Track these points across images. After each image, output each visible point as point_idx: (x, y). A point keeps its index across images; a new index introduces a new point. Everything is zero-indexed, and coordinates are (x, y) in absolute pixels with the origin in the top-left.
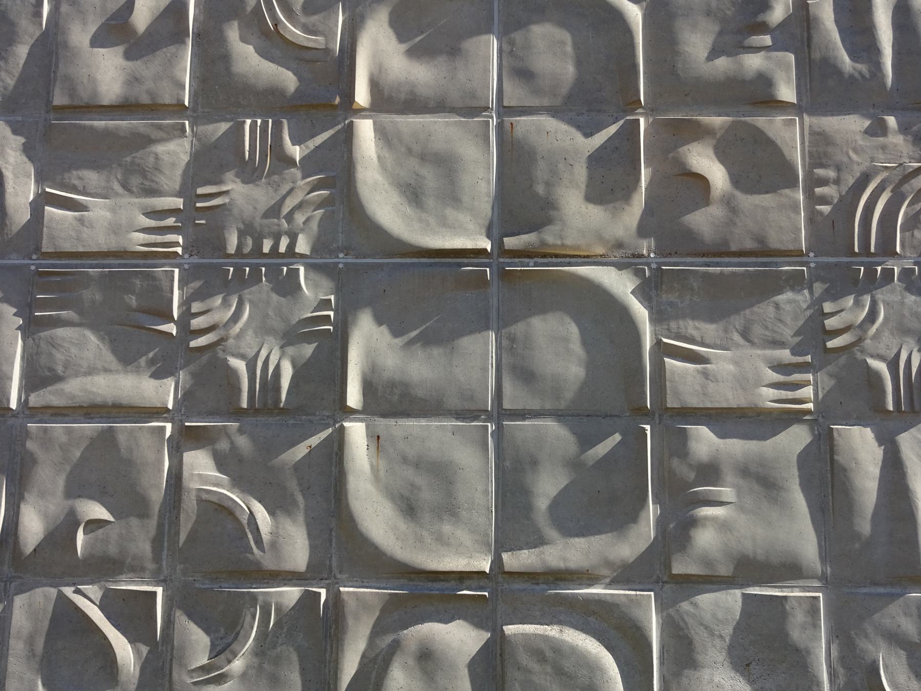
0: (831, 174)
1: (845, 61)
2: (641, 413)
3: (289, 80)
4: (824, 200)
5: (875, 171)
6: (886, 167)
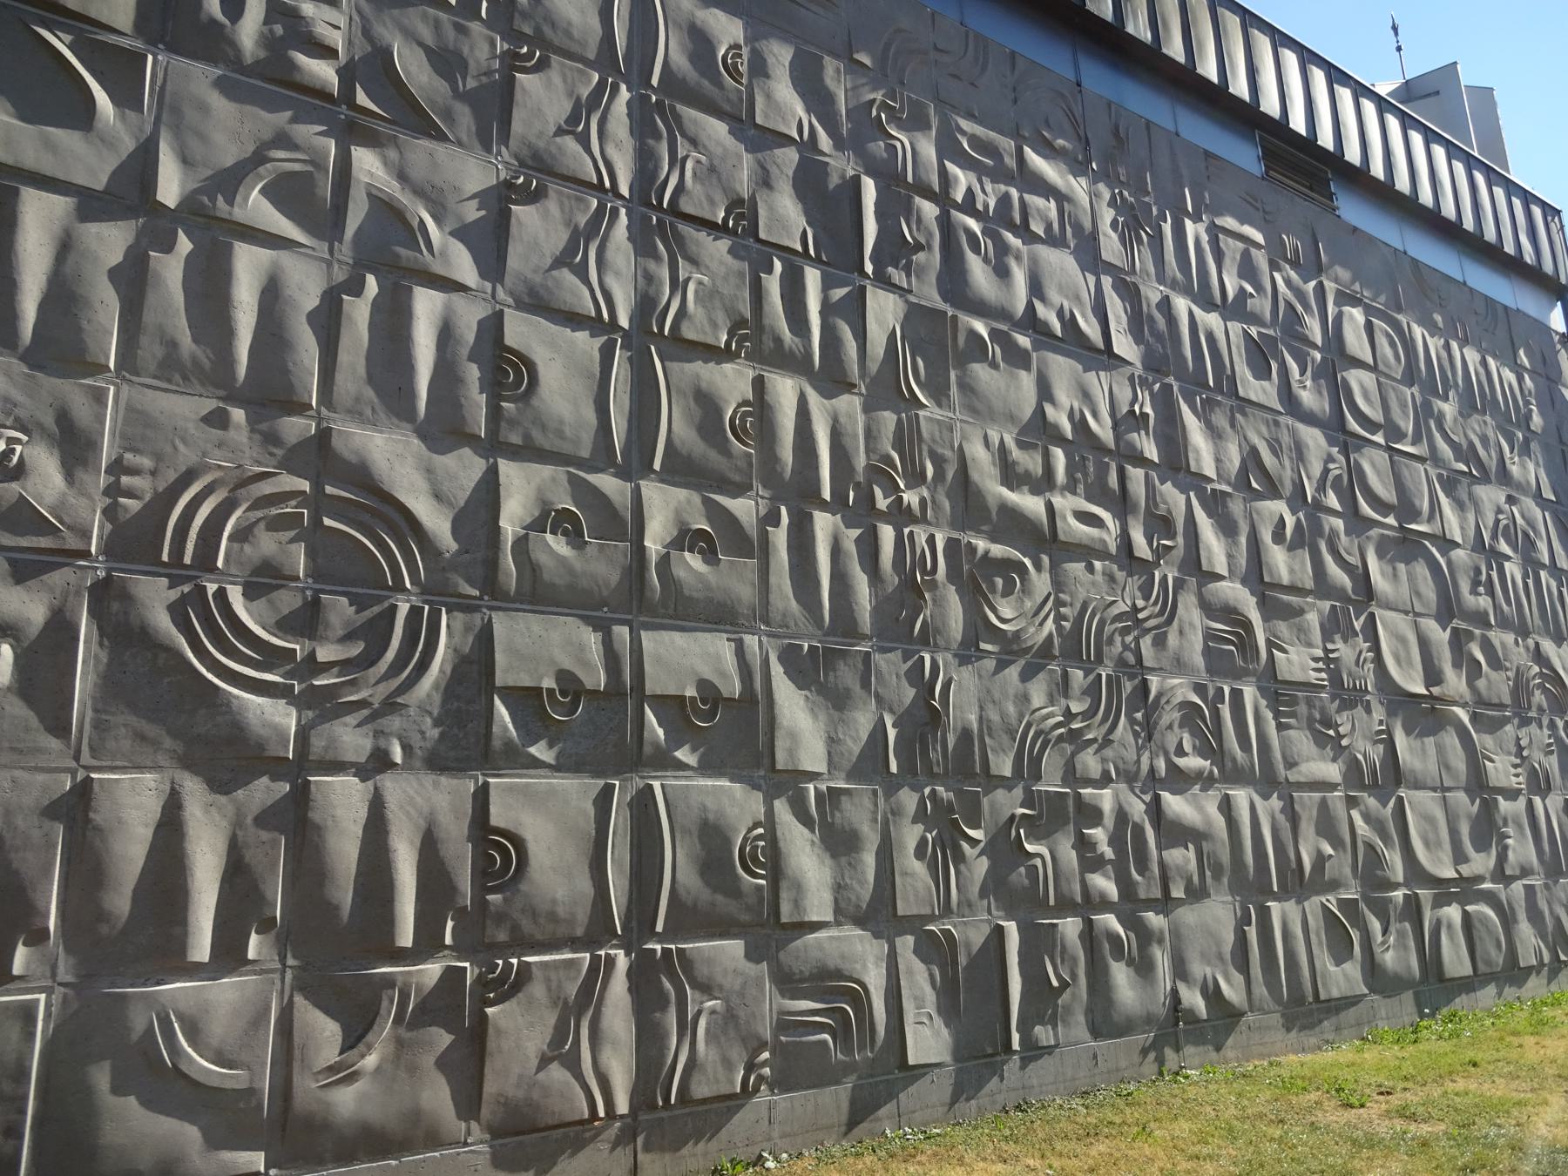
0: (146, 462)
1: (787, 334)
5: (208, 468)
6: (219, 466)
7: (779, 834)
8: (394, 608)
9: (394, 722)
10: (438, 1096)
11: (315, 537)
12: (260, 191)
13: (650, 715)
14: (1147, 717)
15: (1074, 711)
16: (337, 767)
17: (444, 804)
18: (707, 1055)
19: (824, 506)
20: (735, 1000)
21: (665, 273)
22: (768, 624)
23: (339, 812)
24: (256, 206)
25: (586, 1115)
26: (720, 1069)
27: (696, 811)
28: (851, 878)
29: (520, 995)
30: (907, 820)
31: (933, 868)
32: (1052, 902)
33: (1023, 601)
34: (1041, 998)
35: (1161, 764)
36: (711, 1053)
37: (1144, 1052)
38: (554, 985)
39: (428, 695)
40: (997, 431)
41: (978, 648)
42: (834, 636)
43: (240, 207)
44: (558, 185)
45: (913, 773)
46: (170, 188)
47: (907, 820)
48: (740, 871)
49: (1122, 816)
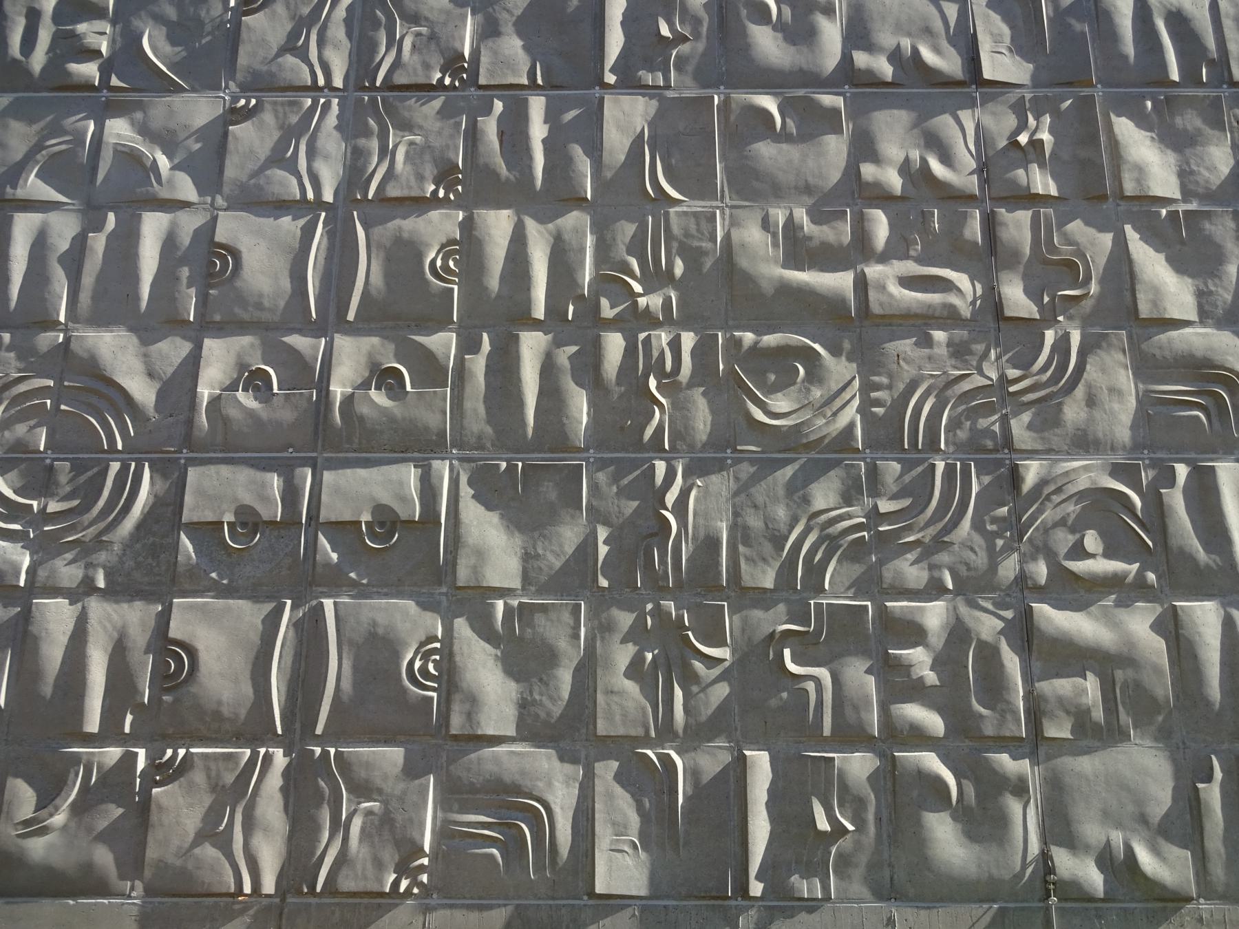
0: (884, 380)
2: (715, 589)
3: (493, 282)
4: (878, 403)
6: (932, 375)
7: (456, 648)
8: (933, 467)
9: (944, 557)
11: (52, 420)
12: (36, 176)
13: (322, 540)
14: (1017, 513)
15: (882, 510)
16: (55, 592)
17: (135, 620)
18: (358, 852)
19: (536, 325)
20: (394, 804)
21: (374, 144)
22: (460, 448)
23: (51, 626)
25: (232, 890)
26: (369, 866)
27: (366, 626)
28: (541, 694)
29: (182, 779)
30: (617, 637)
31: (649, 690)
32: (827, 731)
33: (808, 390)
35: (1041, 571)
36: (363, 850)
38: (213, 774)
39: (968, 534)
40: (785, 207)
41: (735, 450)
42: (540, 452)
43: (22, 188)
44: (272, 97)
45: (624, 592)
47: (617, 637)
48: (407, 683)
49: (958, 633)
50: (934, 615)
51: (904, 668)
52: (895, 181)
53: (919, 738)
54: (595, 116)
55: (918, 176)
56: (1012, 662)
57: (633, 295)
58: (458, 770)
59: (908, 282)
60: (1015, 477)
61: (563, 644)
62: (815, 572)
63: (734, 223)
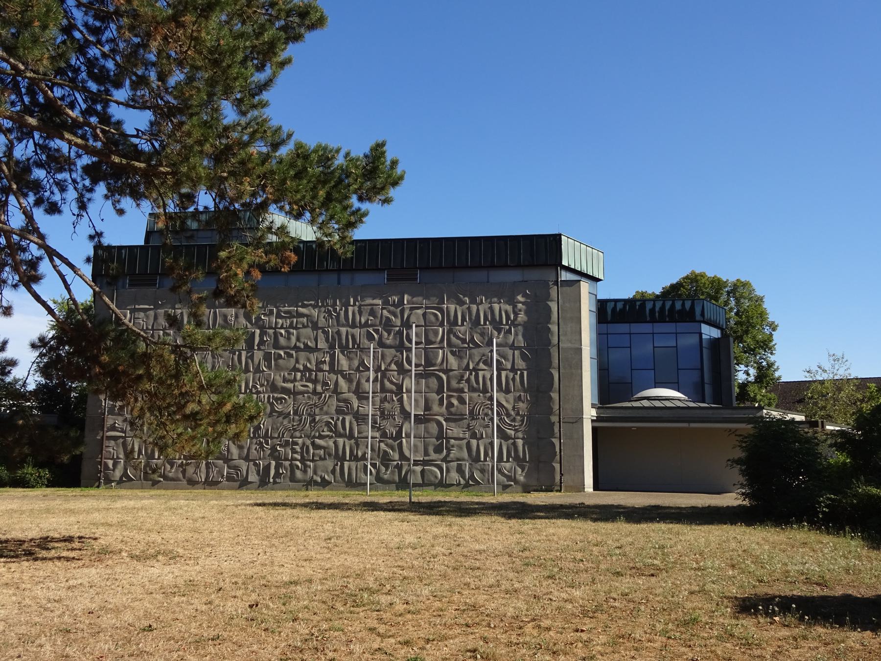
10: (181, 476)
18: (69, 152)
24: (482, 366)
34: (277, 475)
37: (303, 486)
46: (471, 367)
49: (304, 444)
50: (300, 441)
51: (295, 449)
52: (301, 368)
53: (296, 460)
54: (253, 355)
55: (305, 367)
56: (311, 448)
57: (257, 388)
58: (229, 463)
59: (302, 386)
60: (314, 419)
61: (245, 445)
62: (283, 434)
63: (275, 375)
